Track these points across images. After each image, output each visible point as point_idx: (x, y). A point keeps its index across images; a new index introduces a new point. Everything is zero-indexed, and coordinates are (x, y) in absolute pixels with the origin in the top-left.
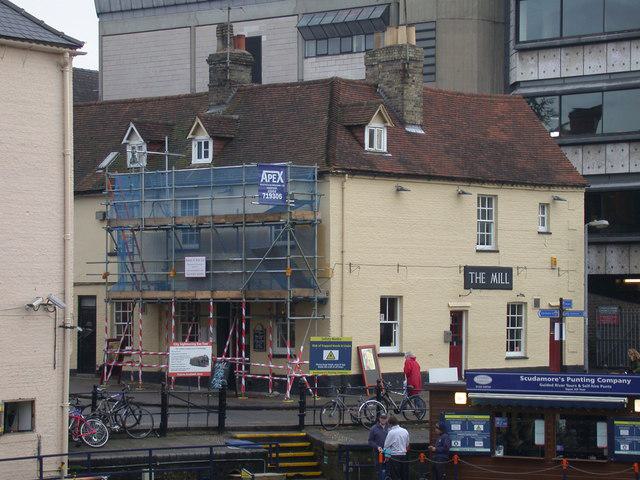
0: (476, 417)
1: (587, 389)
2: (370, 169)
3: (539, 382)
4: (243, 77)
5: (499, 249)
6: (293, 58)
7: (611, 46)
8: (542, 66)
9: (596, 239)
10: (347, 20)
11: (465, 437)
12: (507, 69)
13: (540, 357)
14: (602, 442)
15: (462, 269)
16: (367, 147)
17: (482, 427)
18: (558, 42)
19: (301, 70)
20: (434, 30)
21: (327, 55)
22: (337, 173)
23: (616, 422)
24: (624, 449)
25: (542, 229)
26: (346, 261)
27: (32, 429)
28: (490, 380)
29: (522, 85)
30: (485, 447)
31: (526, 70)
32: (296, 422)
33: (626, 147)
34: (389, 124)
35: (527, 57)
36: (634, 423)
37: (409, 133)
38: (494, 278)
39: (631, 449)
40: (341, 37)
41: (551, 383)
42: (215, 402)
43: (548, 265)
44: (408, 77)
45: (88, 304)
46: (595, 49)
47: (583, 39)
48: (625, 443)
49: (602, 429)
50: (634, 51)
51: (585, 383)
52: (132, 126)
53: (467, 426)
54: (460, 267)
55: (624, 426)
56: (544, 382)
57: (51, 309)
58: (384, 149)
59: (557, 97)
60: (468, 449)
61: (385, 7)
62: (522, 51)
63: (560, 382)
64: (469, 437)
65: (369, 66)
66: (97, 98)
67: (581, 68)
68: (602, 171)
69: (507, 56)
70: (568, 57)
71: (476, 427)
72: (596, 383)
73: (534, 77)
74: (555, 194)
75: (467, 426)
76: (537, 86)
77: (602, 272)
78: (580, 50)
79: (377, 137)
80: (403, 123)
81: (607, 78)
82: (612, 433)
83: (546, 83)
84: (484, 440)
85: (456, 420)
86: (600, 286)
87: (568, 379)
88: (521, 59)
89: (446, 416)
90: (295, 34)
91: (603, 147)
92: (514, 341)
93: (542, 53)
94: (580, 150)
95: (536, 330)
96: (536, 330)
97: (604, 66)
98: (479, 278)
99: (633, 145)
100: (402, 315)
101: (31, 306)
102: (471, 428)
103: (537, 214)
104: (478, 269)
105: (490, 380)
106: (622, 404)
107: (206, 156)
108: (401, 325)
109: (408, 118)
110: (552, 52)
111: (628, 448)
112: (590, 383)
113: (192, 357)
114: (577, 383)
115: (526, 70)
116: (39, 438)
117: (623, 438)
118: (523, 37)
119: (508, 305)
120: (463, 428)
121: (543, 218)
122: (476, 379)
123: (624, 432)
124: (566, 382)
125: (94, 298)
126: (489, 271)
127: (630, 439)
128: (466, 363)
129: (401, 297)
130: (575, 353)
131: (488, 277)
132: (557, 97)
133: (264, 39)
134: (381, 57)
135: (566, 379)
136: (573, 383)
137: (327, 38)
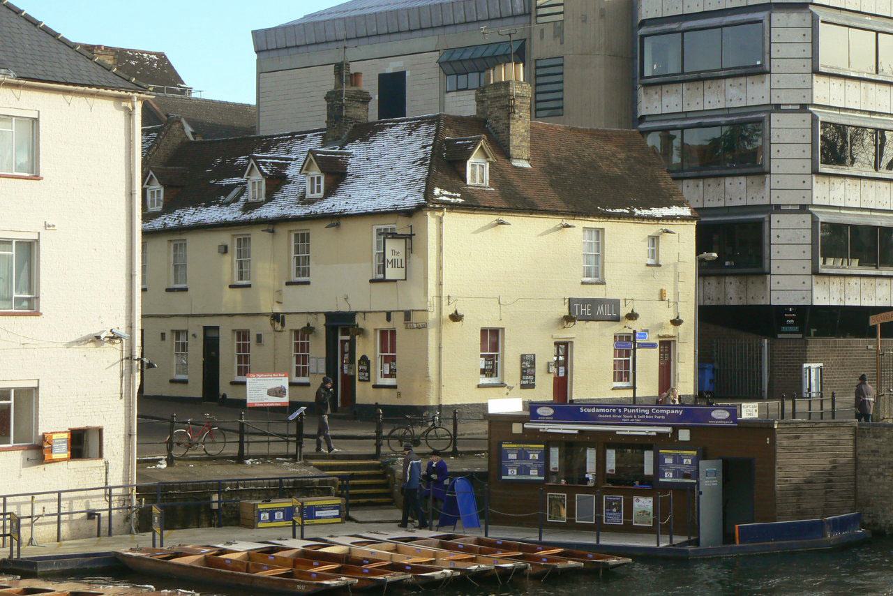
0: (531, 446)
1: (642, 420)
2: (472, 204)
3: (599, 413)
4: (359, 113)
5: (607, 281)
6: (436, 92)
7: (729, 81)
8: (666, 100)
9: (705, 271)
10: (484, 55)
11: (521, 466)
12: (634, 103)
13: (647, 387)
14: (648, 470)
15: (567, 301)
16: (469, 182)
17: (537, 456)
18: (679, 78)
19: (442, 104)
20: (562, 65)
21: (466, 89)
22: (434, 208)
23: (660, 451)
24: (668, 477)
25: (650, 261)
26: (445, 294)
27: (101, 456)
28: (551, 411)
29: (647, 119)
30: (539, 475)
31: (652, 104)
32: (373, 451)
33: (742, 179)
34: (491, 159)
35: (651, 91)
36: (677, 452)
37: (516, 167)
38: (600, 310)
39: (674, 477)
40: (458, 75)
41: (608, 414)
42: (293, 431)
43: (657, 297)
44: (514, 112)
45: (211, 334)
46: (714, 84)
47: (702, 75)
48: (669, 471)
49: (648, 456)
50: (750, 87)
51: (641, 414)
52: (151, 173)
53: (523, 455)
54: (565, 299)
55: (512, 450)
56: (602, 413)
57: (118, 341)
58: (487, 183)
59: (680, 131)
60: (523, 477)
61: (520, 43)
62: (646, 85)
63: (617, 413)
64: (525, 466)
65: (480, 102)
66: (254, 133)
67: (701, 103)
68: (721, 204)
69: (635, 89)
70: (690, 92)
71: (531, 456)
72: (651, 414)
73: (658, 111)
74: (664, 227)
75: (523, 455)
76: (661, 120)
77: (721, 303)
78: (700, 84)
79: (477, 170)
80: (508, 157)
81: (684, 116)
82: (658, 461)
83: (689, 115)
84: (538, 469)
85: (669, 454)
86: (708, 315)
87: (625, 410)
88: (646, 94)
89: (503, 446)
90: (438, 70)
91: (722, 180)
92: (625, 371)
93: (665, 88)
94: (701, 183)
95: (648, 362)
96: (648, 362)
97: (722, 100)
98: (580, 311)
99: (750, 179)
100: (503, 346)
101: (98, 338)
102: (527, 458)
103: (645, 247)
104: (584, 302)
105: (551, 411)
106: (667, 434)
107: (319, 191)
108: (503, 357)
109: (514, 152)
110: (674, 87)
111: (671, 476)
112: (644, 414)
113: (270, 387)
114: (633, 414)
115: (652, 104)
116: (107, 464)
117: (667, 466)
118: (648, 73)
119: (615, 337)
120: (519, 457)
121: (653, 250)
122: (539, 411)
123: (669, 461)
124: (622, 413)
125: (217, 328)
126: (594, 303)
127: (518, 463)
128: (571, 393)
129: (503, 329)
130: (686, 383)
131: (593, 309)
132: (680, 131)
133: (408, 74)
134: (490, 93)
135: (622, 410)
136: (629, 414)
137: (467, 73)
